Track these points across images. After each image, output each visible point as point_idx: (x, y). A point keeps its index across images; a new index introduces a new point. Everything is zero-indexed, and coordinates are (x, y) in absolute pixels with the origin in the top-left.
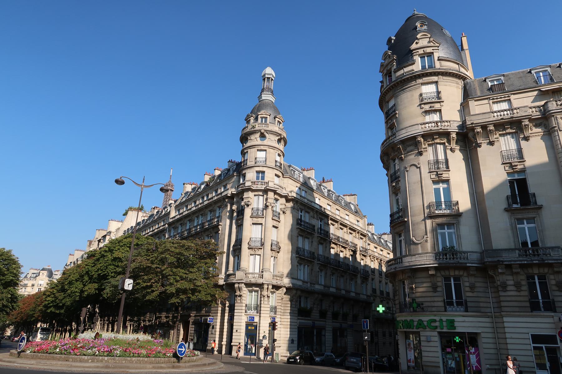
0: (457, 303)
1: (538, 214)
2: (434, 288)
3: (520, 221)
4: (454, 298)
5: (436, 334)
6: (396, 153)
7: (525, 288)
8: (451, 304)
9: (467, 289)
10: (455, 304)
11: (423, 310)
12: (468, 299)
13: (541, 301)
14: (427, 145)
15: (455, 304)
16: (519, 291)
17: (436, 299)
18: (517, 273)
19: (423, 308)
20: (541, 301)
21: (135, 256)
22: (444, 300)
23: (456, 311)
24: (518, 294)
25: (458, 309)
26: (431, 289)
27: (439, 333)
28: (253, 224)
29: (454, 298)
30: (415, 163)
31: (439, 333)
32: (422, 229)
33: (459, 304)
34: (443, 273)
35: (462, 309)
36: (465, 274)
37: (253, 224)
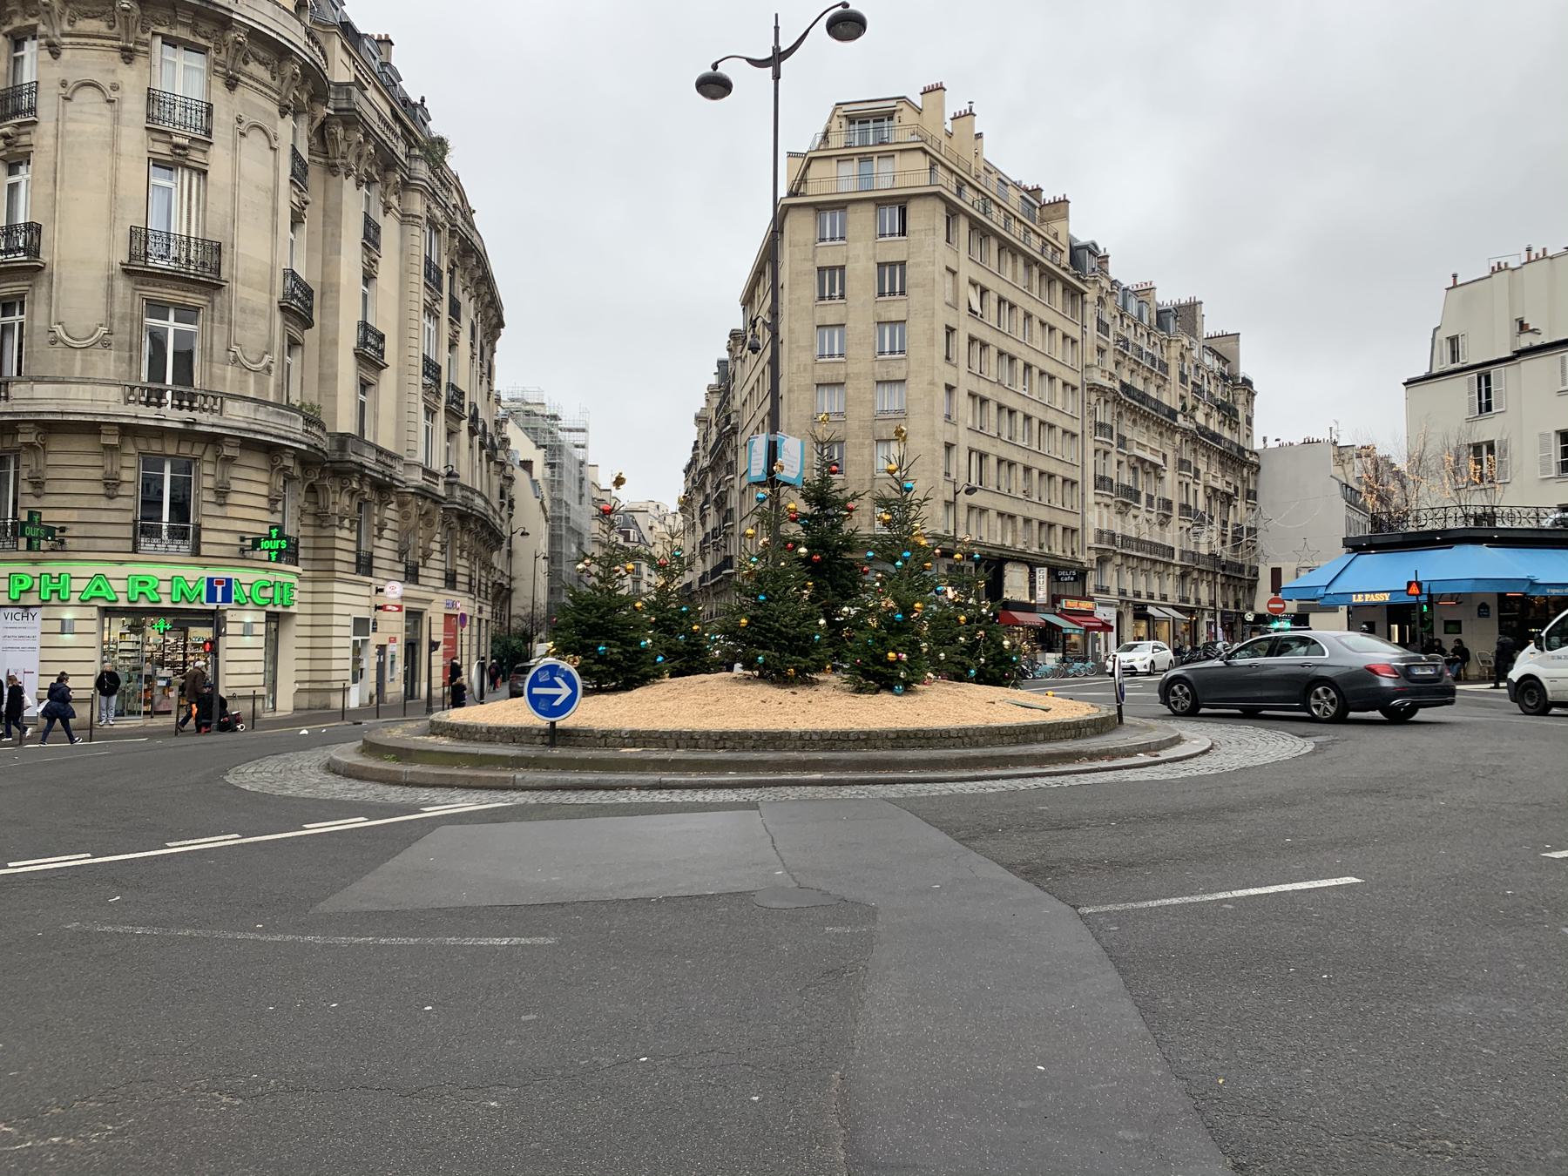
0: (172, 531)
1: (212, 301)
2: (111, 486)
3: (157, 308)
5: (262, 616)
6: (32, 21)
8: (152, 532)
9: (208, 496)
10: (165, 534)
11: (60, 545)
12: (206, 523)
14: (148, 36)
15: (165, 534)
16: (111, 498)
19: (62, 542)
21: (474, 418)
22: (135, 521)
23: (172, 554)
24: (104, 502)
25: (173, 548)
26: (264, 503)
27: (268, 613)
28: (583, 430)
30: (261, 123)
31: (268, 613)
32: (746, 503)
33: (179, 534)
34: (142, 446)
35: (184, 548)
36: (208, 456)
37: (583, 430)
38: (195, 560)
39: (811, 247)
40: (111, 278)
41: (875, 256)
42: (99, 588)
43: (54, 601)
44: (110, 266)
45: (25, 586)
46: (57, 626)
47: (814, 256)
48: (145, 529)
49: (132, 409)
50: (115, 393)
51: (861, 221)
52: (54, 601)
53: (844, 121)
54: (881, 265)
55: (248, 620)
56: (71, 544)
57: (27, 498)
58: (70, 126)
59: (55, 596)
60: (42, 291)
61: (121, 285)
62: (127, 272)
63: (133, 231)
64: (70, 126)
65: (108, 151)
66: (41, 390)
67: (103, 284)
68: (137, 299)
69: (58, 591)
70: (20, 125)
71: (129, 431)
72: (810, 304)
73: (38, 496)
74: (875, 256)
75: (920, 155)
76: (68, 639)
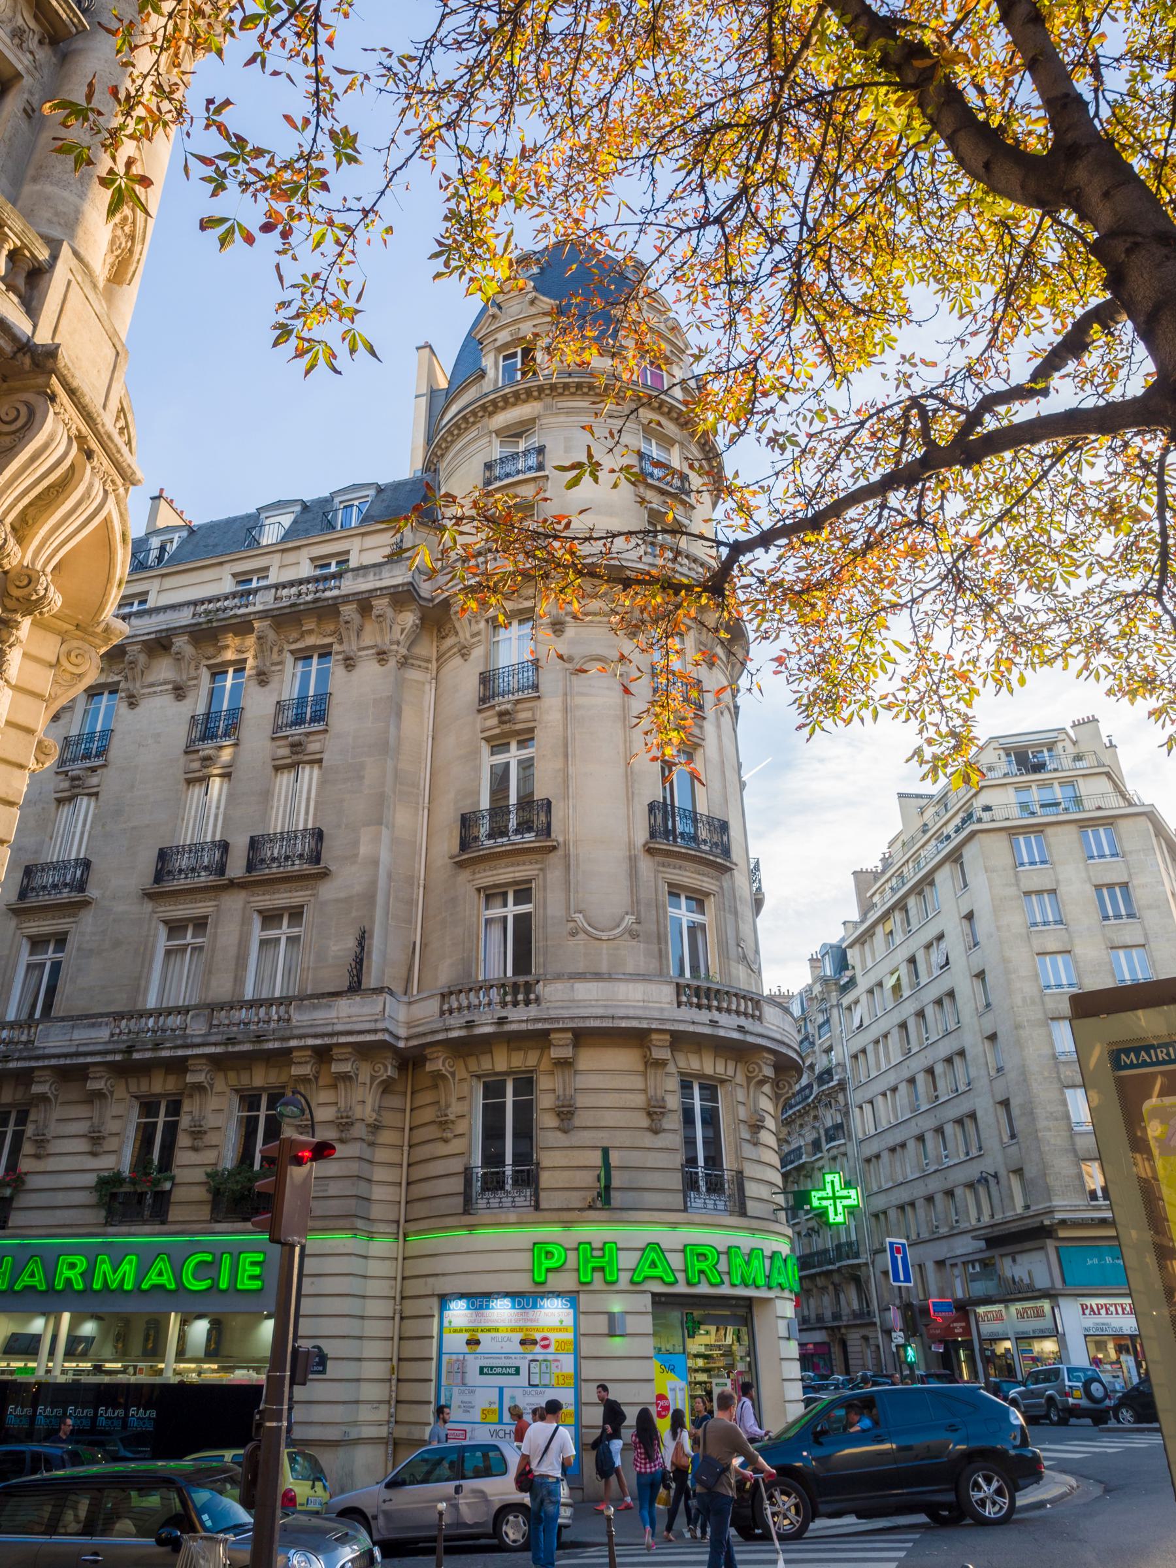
2: (654, 1112)
4: (509, 1159)
7: (674, 1122)
8: (494, 1183)
13: (509, 1170)
16: (656, 1132)
17: (652, 1160)
18: (660, 1064)
20: (509, 1170)
24: (648, 1140)
29: (509, 1159)
36: (740, 1078)
38: (743, 1222)
39: (1011, 873)
40: (632, 860)
41: (1089, 878)
42: (653, 1265)
43: (598, 1285)
44: (631, 845)
45: (552, 1263)
46: (601, 1324)
47: (1017, 879)
48: (690, 1184)
49: (687, 1013)
50: (666, 993)
51: (1063, 841)
52: (598, 1285)
53: (1002, 752)
54: (1098, 888)
55: (616, 1308)
56: (175, 1213)
57: (28, 1160)
58: (579, 700)
59: (598, 1275)
60: (554, 875)
61: (646, 865)
62: (650, 851)
63: (652, 807)
64: (579, 700)
65: (619, 725)
66: (587, 991)
67: (625, 866)
68: (660, 882)
69: (602, 1269)
70: (518, 701)
71: (680, 1040)
72: (1024, 931)
73: (565, 1132)
74: (1089, 878)
75: (1104, 779)
76: (617, 1344)
